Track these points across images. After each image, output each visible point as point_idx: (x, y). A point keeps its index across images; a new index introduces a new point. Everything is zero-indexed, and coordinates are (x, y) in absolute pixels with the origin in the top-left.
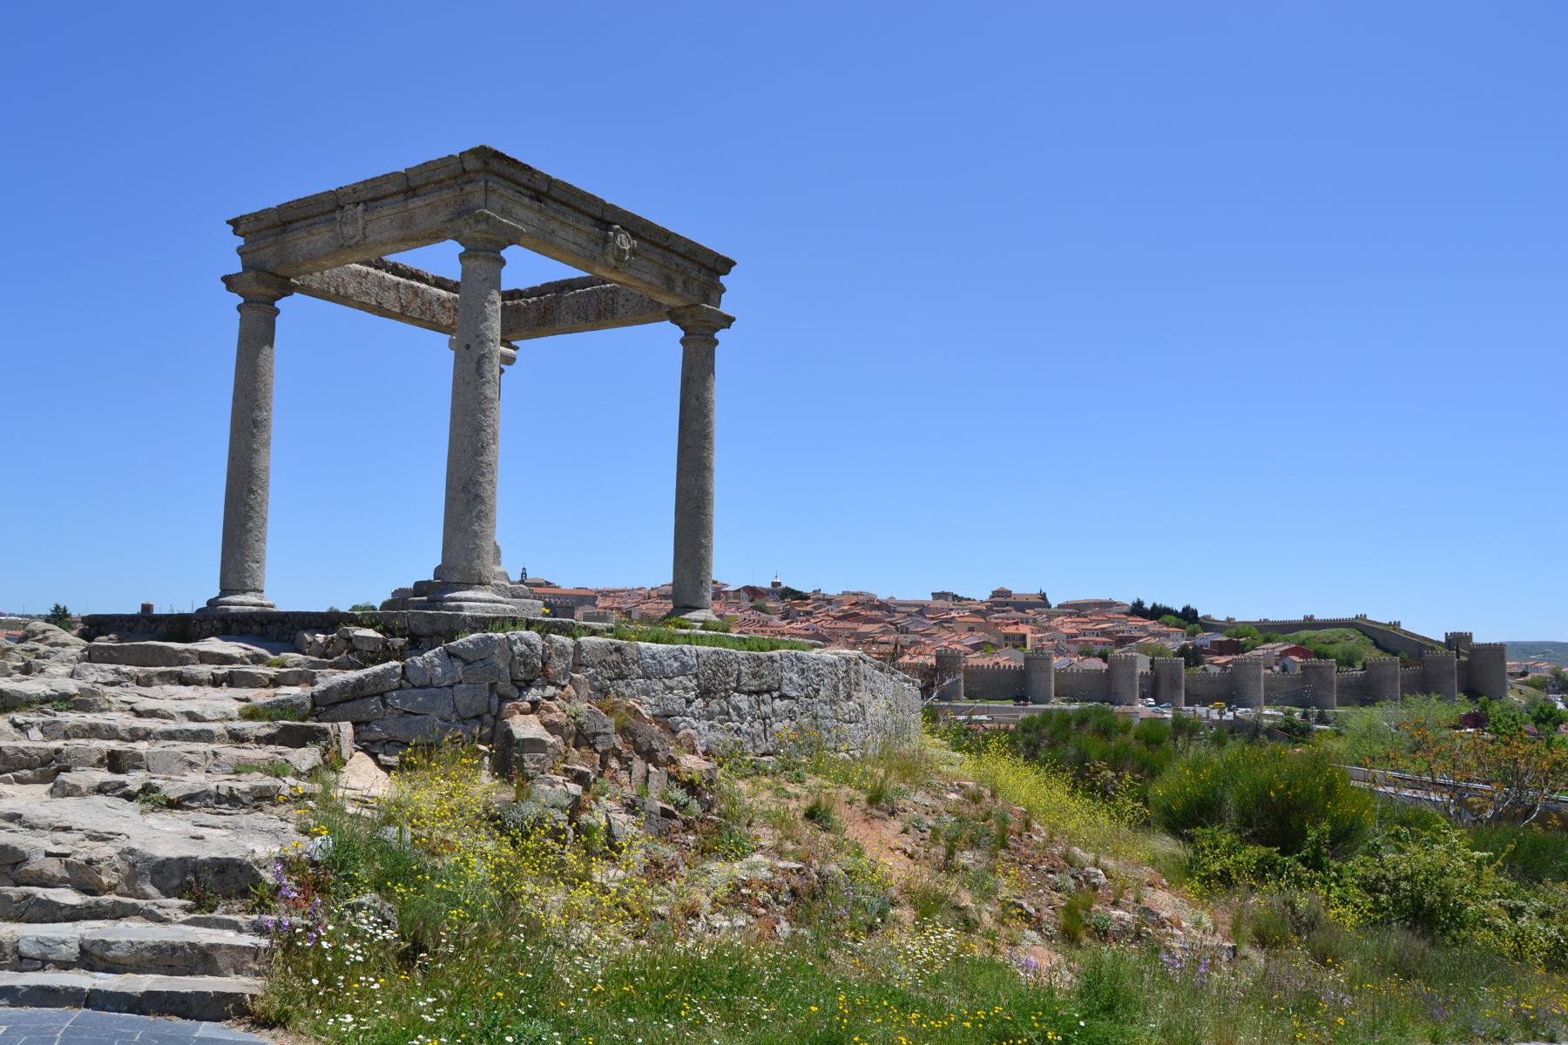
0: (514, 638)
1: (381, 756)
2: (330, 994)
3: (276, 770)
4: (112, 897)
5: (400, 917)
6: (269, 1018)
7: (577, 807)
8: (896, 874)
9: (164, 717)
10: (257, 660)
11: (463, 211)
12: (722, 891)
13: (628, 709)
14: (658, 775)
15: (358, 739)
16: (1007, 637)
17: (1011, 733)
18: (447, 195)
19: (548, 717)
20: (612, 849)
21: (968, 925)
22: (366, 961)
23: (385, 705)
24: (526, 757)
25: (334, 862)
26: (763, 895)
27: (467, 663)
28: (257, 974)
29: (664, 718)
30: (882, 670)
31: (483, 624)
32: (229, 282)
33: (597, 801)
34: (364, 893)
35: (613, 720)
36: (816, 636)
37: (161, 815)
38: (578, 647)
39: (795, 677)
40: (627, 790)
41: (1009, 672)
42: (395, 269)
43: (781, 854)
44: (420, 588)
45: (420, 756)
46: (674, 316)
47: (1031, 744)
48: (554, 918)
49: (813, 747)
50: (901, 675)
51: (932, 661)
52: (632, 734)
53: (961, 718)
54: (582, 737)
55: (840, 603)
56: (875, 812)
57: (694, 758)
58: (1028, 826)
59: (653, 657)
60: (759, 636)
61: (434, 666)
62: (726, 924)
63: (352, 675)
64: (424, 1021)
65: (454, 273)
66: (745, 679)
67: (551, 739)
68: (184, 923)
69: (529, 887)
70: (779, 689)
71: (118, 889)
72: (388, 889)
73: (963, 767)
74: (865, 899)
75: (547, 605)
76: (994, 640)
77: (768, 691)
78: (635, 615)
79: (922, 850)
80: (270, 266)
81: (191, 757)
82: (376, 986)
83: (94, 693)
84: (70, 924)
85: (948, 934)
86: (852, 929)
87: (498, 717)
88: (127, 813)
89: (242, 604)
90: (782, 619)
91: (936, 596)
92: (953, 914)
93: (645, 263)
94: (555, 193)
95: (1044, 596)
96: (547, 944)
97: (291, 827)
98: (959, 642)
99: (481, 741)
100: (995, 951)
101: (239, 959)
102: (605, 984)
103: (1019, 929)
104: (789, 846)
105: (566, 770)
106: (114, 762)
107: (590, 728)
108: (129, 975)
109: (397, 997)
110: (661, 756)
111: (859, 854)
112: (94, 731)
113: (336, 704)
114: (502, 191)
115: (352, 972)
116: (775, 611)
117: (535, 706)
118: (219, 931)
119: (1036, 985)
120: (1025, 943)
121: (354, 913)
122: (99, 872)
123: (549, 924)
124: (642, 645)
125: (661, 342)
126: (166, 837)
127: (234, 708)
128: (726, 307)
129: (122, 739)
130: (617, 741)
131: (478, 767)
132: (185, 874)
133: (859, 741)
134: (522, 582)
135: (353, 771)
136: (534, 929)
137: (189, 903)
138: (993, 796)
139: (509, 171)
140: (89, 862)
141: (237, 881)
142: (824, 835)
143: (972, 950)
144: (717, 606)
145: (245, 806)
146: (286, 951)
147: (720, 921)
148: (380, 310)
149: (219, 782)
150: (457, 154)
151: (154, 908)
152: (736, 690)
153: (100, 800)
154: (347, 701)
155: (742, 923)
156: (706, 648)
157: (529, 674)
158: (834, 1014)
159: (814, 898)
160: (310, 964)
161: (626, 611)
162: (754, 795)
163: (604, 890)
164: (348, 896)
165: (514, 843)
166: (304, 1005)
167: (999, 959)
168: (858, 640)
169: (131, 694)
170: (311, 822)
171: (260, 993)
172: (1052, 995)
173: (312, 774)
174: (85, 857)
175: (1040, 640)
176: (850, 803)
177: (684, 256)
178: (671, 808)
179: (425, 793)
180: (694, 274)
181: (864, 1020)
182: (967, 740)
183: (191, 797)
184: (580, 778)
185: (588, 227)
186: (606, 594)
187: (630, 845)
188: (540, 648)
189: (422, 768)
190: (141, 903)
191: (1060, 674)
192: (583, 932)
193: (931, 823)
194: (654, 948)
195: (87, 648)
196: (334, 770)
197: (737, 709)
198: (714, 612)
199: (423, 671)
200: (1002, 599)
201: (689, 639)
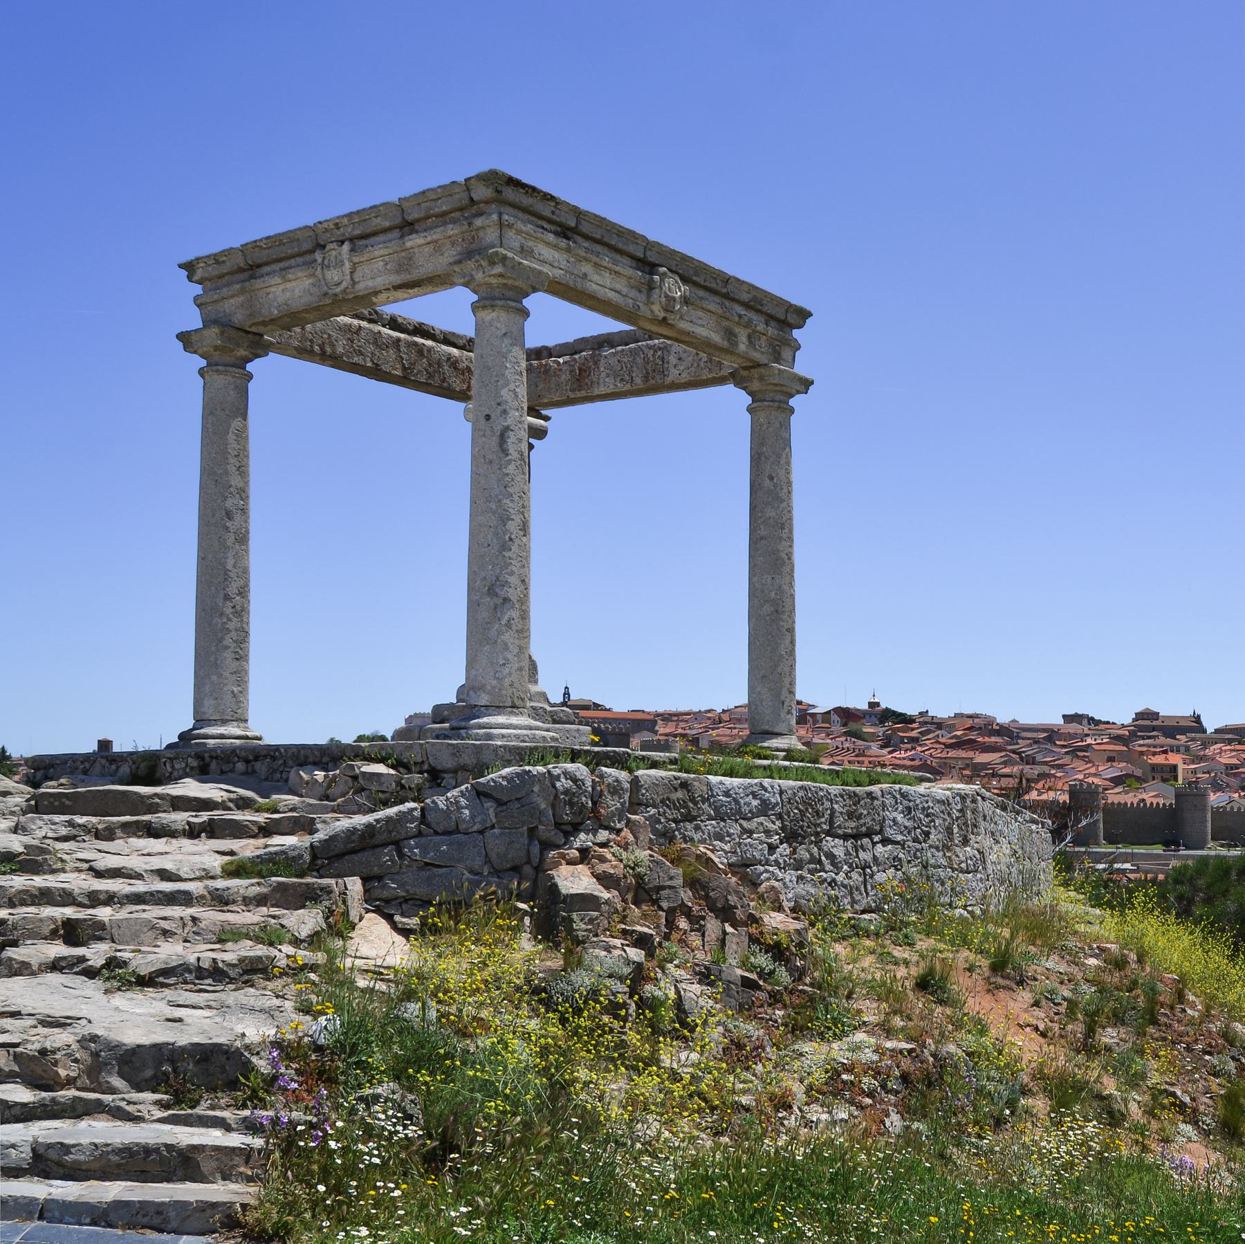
0: (556, 772)
1: (397, 918)
2: (340, 1203)
3: (268, 936)
4: (72, 1093)
5: (425, 1111)
6: (264, 1230)
7: (639, 976)
8: (1027, 1057)
9: (131, 877)
10: (243, 804)
11: (473, 251)
12: (819, 1077)
13: (698, 857)
14: (736, 939)
15: (368, 897)
16: (1155, 768)
17: (1160, 884)
18: (452, 230)
19: (601, 868)
20: (683, 1026)
21: (1113, 1118)
22: (385, 1163)
23: (401, 855)
24: (575, 916)
25: (343, 1046)
26: (867, 1082)
27: (500, 803)
28: (250, 1179)
29: (742, 867)
30: (1004, 808)
31: (520, 755)
32: (186, 339)
33: (663, 969)
34: (380, 1082)
35: (680, 871)
36: (924, 767)
37: (129, 994)
38: (635, 782)
39: (900, 818)
40: (700, 955)
41: (1156, 810)
42: (394, 324)
43: (889, 1032)
44: (440, 714)
45: (445, 918)
46: (737, 378)
47: (1184, 898)
48: (615, 1111)
49: (925, 902)
50: (1028, 815)
51: (1065, 798)
52: (705, 887)
53: (1101, 866)
54: (642, 891)
55: (952, 728)
56: (1000, 981)
57: (779, 917)
58: (1181, 997)
59: (727, 794)
60: (855, 767)
61: (459, 808)
62: (824, 1117)
63: (360, 820)
64: (456, 1234)
65: (465, 326)
66: (839, 820)
67: (605, 895)
68: (161, 1121)
69: (583, 1074)
70: (881, 832)
71: (79, 1083)
72: (410, 1076)
73: (1103, 927)
74: (991, 1087)
75: (596, 732)
76: (1138, 772)
77: (869, 835)
78: (704, 743)
79: (1056, 1027)
80: (239, 318)
81: (165, 925)
82: (397, 1193)
83: (43, 851)
84: (20, 1125)
85: (1090, 1129)
86: (976, 1123)
87: (541, 869)
88: (89, 993)
89: (222, 737)
90: (882, 747)
91: (1068, 718)
92: (1095, 1104)
93: (700, 313)
94: (585, 228)
95: (1197, 719)
96: (607, 1141)
97: (289, 1005)
98: (1098, 774)
99: (520, 898)
100: (1145, 1149)
101: (226, 1163)
102: (678, 1190)
103: (1173, 1123)
104: (898, 1022)
105: (624, 932)
106: (71, 933)
107: (653, 880)
108: (93, 1182)
109: (423, 1206)
110: (740, 914)
111: (983, 1032)
112: (45, 897)
113: (340, 856)
114: (520, 225)
115: (366, 1177)
116: (873, 737)
117: (585, 855)
118: (203, 1130)
119: (1192, 1189)
120: (1180, 1139)
121: (368, 1108)
122: (56, 1063)
123: (608, 1118)
124: (714, 779)
125: (729, 405)
126: (136, 1020)
127: (216, 863)
128: (803, 366)
129: (80, 905)
130: (686, 896)
131: (517, 930)
132: (161, 1064)
133: (978, 894)
134: (564, 704)
135: (364, 937)
136: (590, 1124)
137: (165, 1097)
138: (1140, 960)
139: (526, 201)
140: (43, 1052)
141: (223, 1070)
142: (939, 1009)
143: (1118, 1148)
144: (802, 732)
145: (232, 980)
146: (285, 1153)
147: (817, 1114)
148: (376, 373)
149: (200, 953)
150: (461, 179)
151: (123, 1104)
152: (828, 833)
153: (55, 978)
154: (354, 851)
155: (844, 1116)
156: (791, 783)
157: (576, 816)
158: (957, 1226)
159: (930, 1085)
160: (315, 1167)
161: (696, 737)
162: (855, 961)
163: (675, 1077)
164: (360, 1086)
165: (563, 1021)
166: (308, 1216)
167: (1149, 1158)
168: (975, 772)
169: (89, 850)
170: (314, 998)
171: (253, 1202)
172: (1211, 1202)
173: (314, 941)
174: (37, 1046)
175: (1194, 772)
176: (970, 969)
177: (747, 305)
178: (754, 976)
179: (453, 961)
180: (761, 327)
181: (994, 1234)
182: (1109, 894)
183: (166, 972)
184: (642, 941)
185: (627, 269)
186: (667, 717)
187: (705, 1023)
188: (589, 783)
189: (448, 931)
190: (107, 1098)
191: (1218, 813)
192: (651, 1127)
193: (1067, 994)
194: (738, 1146)
195: (33, 797)
196: (340, 935)
197: (831, 856)
198: (800, 738)
199: (447, 813)
200: (1147, 722)
201: (770, 772)
